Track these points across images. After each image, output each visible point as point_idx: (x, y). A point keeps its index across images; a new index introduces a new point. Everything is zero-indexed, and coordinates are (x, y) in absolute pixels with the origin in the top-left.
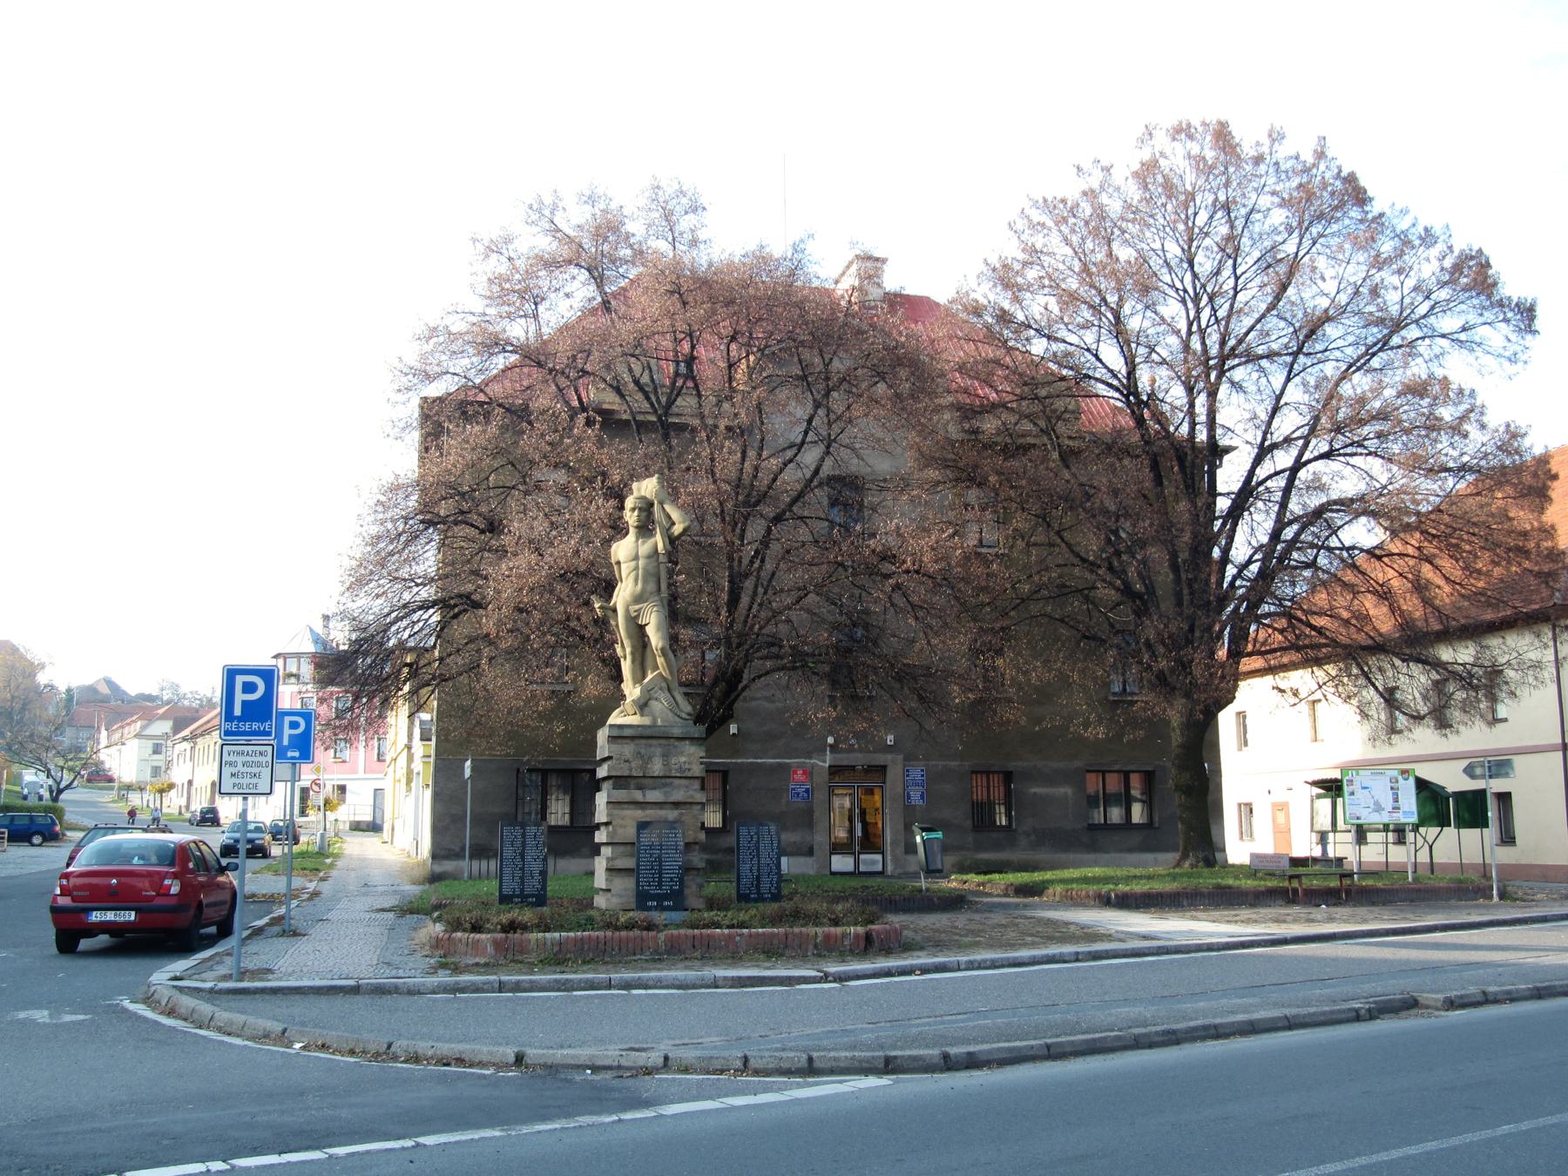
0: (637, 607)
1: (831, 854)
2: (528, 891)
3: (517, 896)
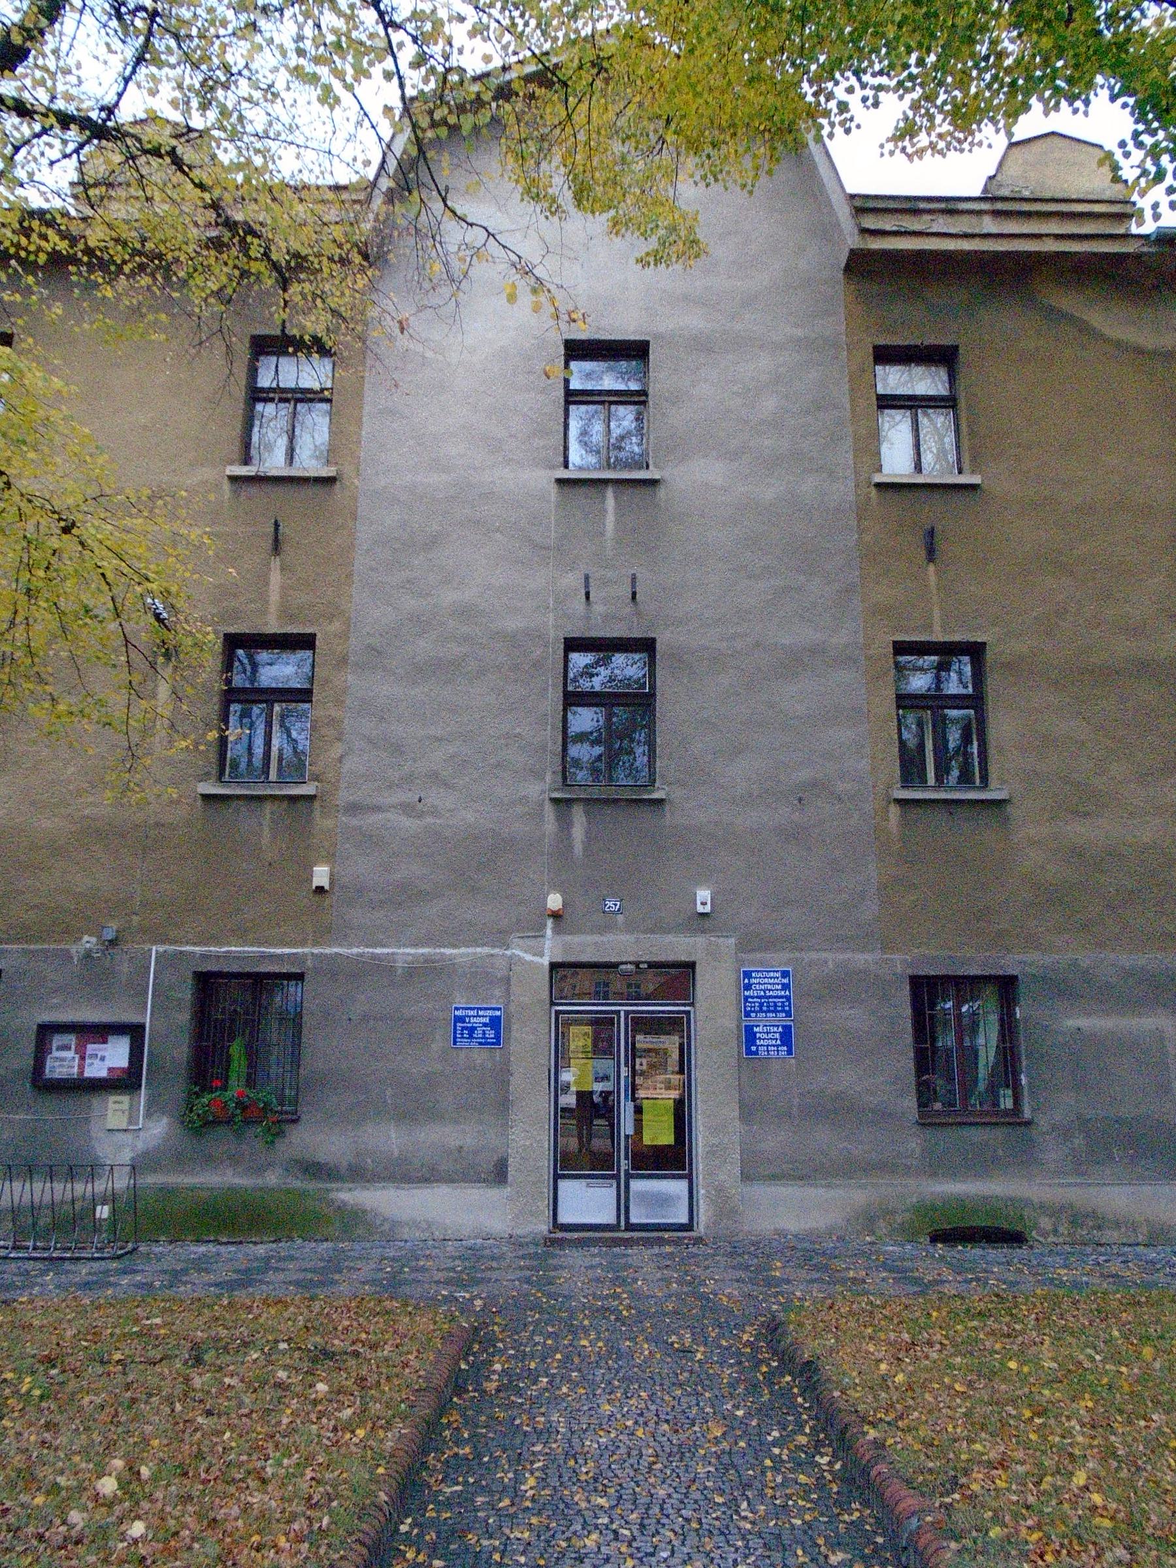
1: (557, 1177)
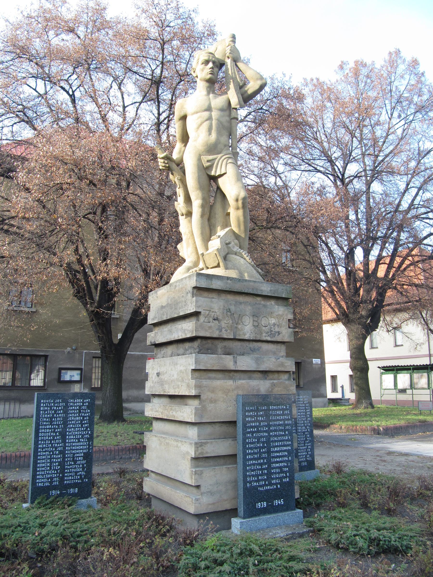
0: (211, 157)
2: (69, 479)
3: (55, 488)
